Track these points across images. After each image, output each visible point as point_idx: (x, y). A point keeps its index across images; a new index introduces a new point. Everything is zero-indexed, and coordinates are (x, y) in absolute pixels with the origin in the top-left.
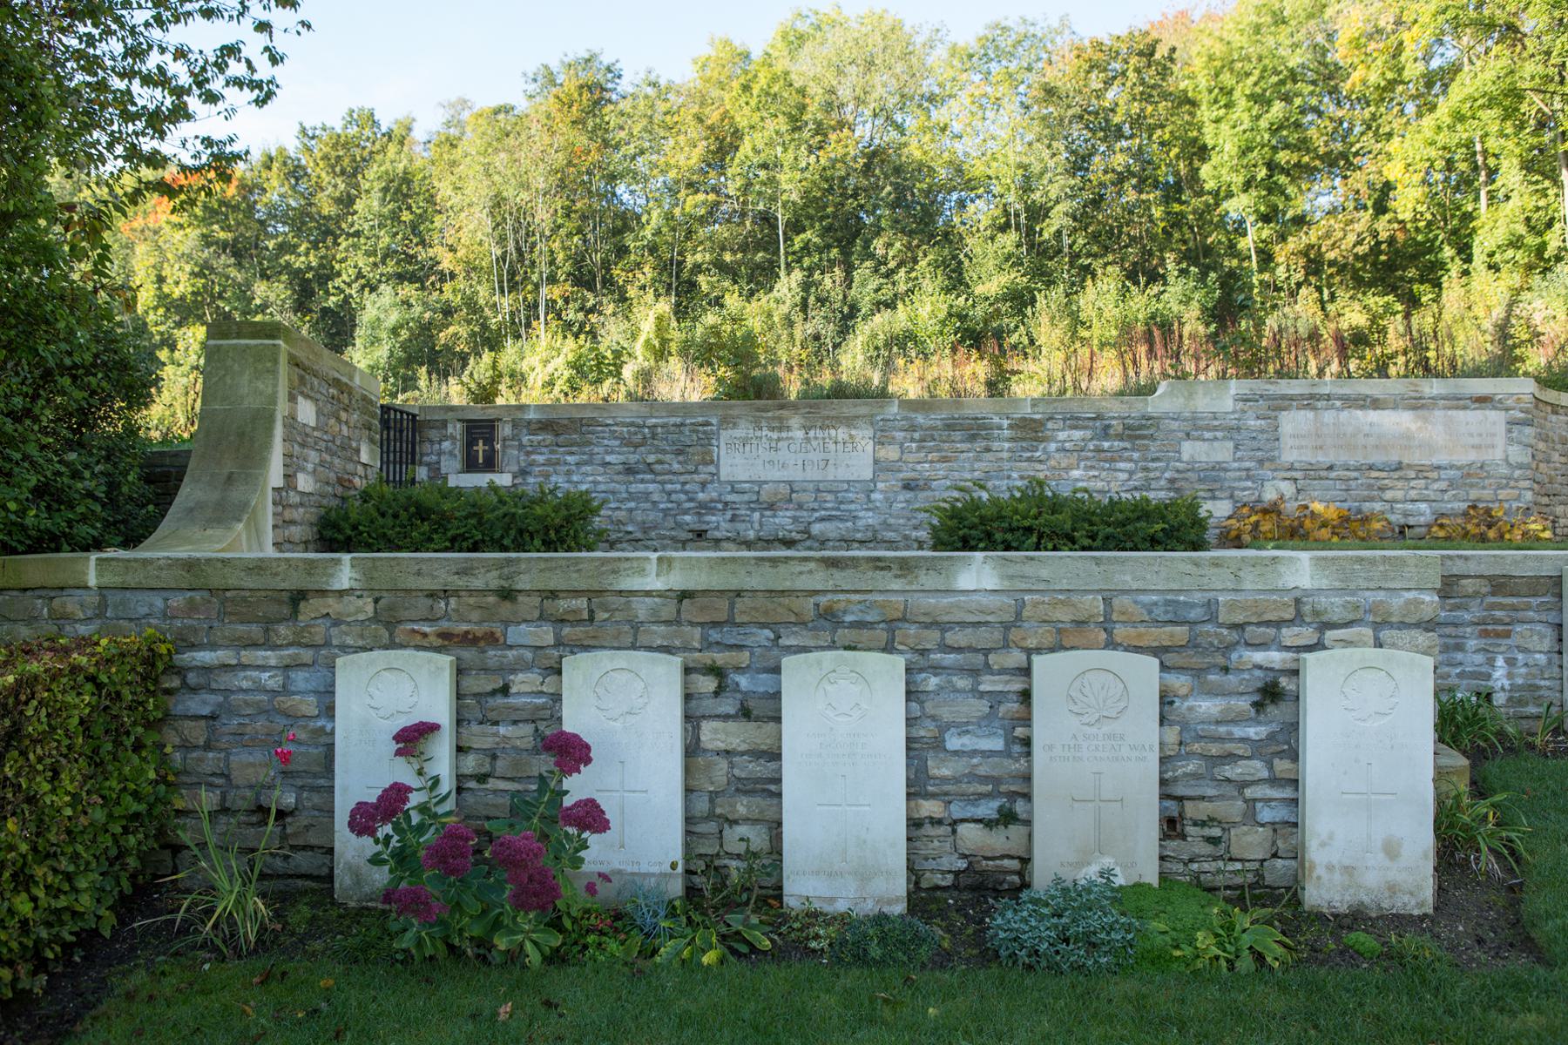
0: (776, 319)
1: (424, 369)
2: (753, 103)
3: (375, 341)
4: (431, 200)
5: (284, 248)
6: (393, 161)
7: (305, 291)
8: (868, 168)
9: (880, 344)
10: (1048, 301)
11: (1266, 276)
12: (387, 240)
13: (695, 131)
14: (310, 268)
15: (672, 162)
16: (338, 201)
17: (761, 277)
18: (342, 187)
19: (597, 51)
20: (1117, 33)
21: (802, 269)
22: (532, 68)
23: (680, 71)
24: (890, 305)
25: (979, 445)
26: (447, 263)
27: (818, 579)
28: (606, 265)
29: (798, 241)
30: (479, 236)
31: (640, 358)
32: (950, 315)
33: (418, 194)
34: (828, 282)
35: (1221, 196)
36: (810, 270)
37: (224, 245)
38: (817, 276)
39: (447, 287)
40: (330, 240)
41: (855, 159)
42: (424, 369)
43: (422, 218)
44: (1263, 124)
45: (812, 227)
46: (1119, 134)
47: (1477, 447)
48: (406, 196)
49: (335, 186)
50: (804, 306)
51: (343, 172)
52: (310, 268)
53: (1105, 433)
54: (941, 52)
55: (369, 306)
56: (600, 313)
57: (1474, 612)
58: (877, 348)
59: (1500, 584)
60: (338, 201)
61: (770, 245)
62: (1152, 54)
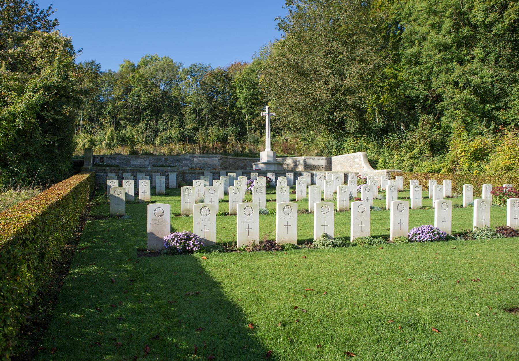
0: (139, 132)
2: (135, 81)
9: (164, 139)
10: (202, 130)
11: (250, 127)
13: (120, 86)
17: (136, 122)
19: (94, 60)
21: (146, 120)
23: (116, 69)
24: (166, 130)
28: (97, 116)
31: (107, 140)
32: (179, 133)
34: (152, 123)
35: (242, 108)
36: (148, 121)
38: (149, 122)
41: (159, 95)
44: (249, 94)
46: (219, 93)
50: (146, 129)
53: (175, 160)
54: (181, 69)
57: (197, 175)
58: (163, 140)
59: (199, 173)
61: (138, 113)
62: (227, 76)
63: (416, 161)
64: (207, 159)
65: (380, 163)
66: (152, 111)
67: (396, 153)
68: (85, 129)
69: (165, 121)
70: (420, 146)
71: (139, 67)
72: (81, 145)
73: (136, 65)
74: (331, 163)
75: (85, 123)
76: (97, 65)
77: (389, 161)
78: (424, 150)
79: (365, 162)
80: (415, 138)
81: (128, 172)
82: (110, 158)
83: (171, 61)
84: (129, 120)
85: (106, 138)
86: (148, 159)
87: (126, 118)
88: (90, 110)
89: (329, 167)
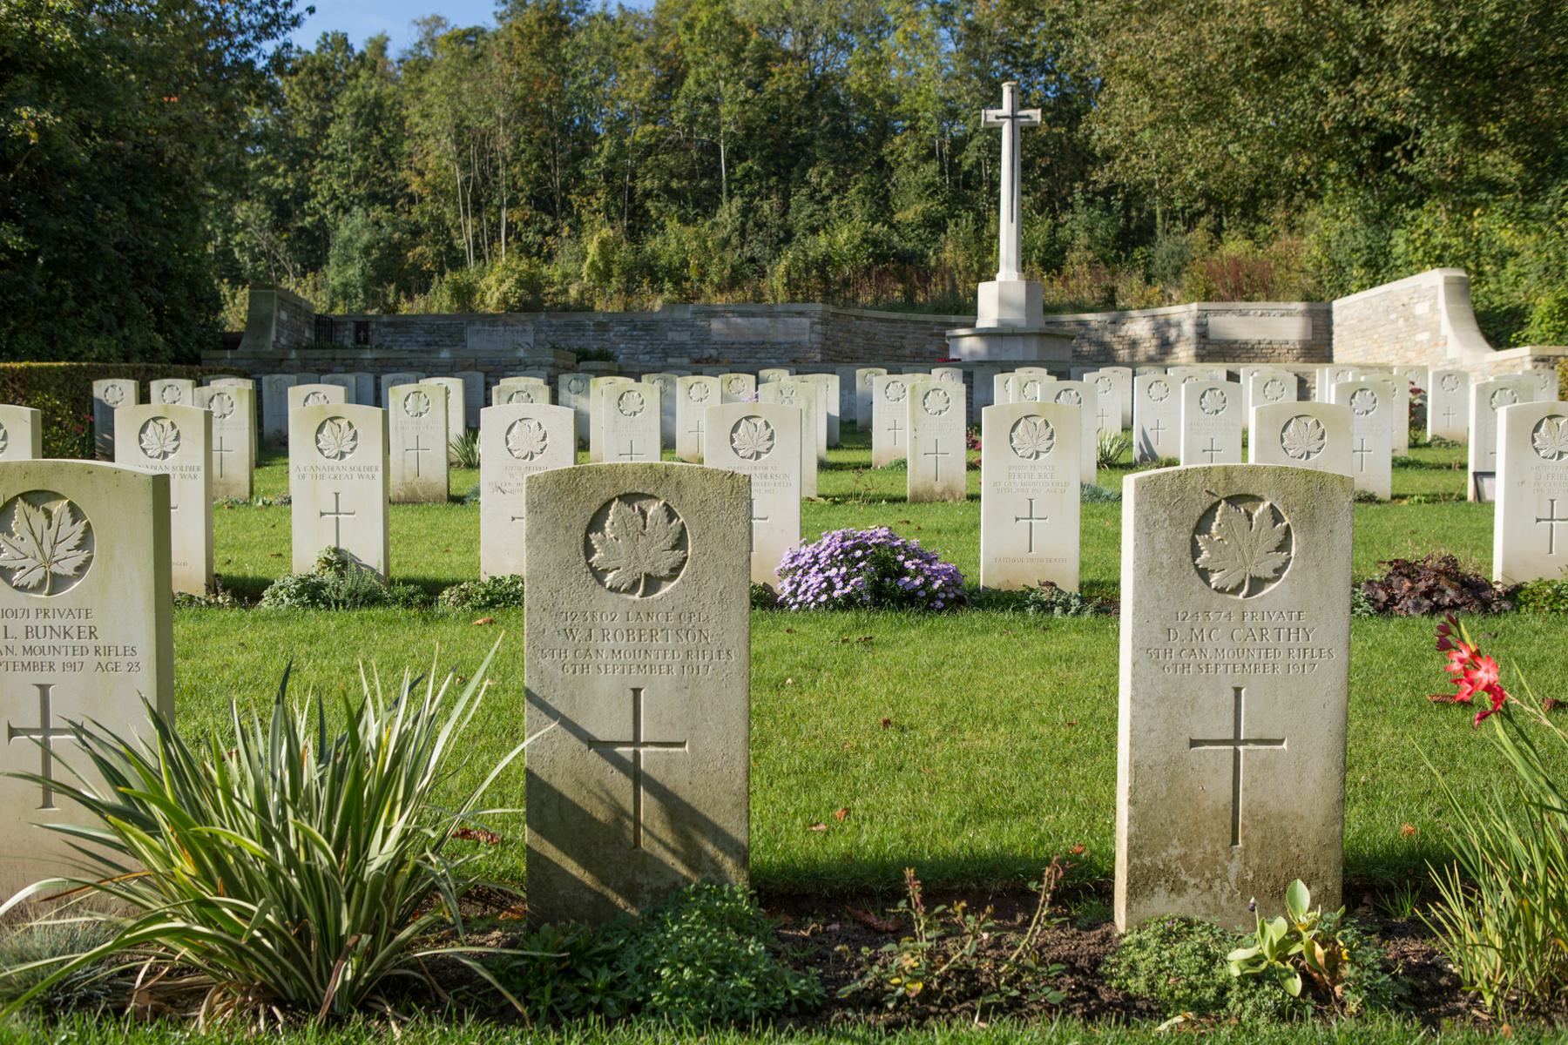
1: (393, 287)
3: (348, 260)
6: (368, 86)
7: (283, 209)
8: (810, 98)
14: (287, 189)
15: (624, 94)
16: (314, 124)
17: (706, 203)
18: (316, 111)
25: (581, 333)
26: (415, 186)
27: (408, 355)
28: (565, 188)
30: (445, 162)
31: (585, 280)
32: (865, 240)
33: (388, 119)
34: (766, 207)
38: (756, 202)
39: (415, 209)
40: (306, 164)
42: (393, 287)
43: (390, 142)
45: (753, 157)
47: (797, 334)
48: (378, 119)
49: (310, 110)
51: (317, 96)
52: (287, 189)
53: (635, 328)
55: (342, 227)
60: (314, 124)
61: (712, 171)
64: (767, 320)
65: (1536, 318)
66: (769, 158)
68: (518, 238)
69: (818, 196)
72: (495, 301)
74: (1330, 333)
75: (517, 215)
79: (1452, 319)
81: (364, 370)
84: (675, 195)
85: (585, 269)
86: (530, 328)
87: (667, 189)
88: (535, 165)
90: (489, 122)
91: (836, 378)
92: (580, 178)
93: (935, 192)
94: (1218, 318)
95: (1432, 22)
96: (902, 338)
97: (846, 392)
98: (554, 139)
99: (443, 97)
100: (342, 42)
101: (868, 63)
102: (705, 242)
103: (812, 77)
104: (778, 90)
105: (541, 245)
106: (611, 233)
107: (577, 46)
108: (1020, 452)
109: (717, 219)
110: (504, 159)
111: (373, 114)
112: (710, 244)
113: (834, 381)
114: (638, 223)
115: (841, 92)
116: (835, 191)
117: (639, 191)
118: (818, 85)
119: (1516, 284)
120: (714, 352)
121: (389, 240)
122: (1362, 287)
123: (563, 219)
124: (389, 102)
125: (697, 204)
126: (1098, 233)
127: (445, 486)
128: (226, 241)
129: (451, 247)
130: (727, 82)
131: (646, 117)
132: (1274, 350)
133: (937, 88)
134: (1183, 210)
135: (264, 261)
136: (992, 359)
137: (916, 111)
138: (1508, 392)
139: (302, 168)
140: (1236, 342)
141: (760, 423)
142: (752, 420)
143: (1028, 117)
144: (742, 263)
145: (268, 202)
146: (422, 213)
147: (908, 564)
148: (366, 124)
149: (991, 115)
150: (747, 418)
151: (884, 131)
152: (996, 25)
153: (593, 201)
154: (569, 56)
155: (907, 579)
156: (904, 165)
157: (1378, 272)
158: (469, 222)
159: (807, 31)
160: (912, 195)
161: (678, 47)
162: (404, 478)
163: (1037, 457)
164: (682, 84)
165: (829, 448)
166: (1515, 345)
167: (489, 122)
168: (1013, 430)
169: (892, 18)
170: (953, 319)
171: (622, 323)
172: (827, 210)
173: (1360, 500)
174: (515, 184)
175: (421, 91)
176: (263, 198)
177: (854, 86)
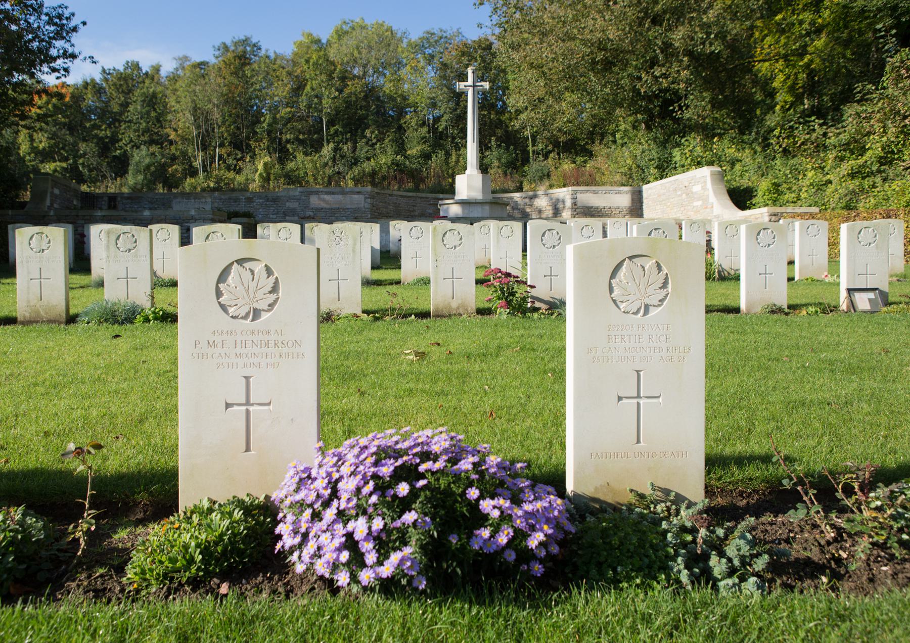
4: (165, 107)
5: (95, 126)
7: (105, 147)
8: (366, 97)
12: (144, 124)
15: (276, 93)
16: (121, 105)
17: (317, 146)
18: (123, 99)
19: (249, 36)
20: (475, 39)
21: (334, 142)
22: (218, 43)
29: (332, 130)
30: (187, 125)
32: (393, 163)
33: (159, 103)
34: (345, 148)
36: (339, 143)
37: (64, 124)
39: (173, 148)
40: (117, 124)
42: (161, 185)
45: (339, 124)
48: (155, 104)
49: (119, 98)
51: (123, 92)
52: (107, 137)
53: (268, 200)
56: (243, 161)
60: (121, 105)
63: (867, 183)
64: (340, 197)
65: (760, 193)
67: (809, 166)
68: (224, 162)
69: (370, 143)
70: (885, 139)
71: (329, 43)
73: (324, 41)
75: (223, 151)
76: (254, 45)
77: (789, 189)
78: (900, 151)
80: (868, 119)
82: (128, 198)
83: (390, 29)
84: (301, 142)
87: (297, 139)
89: (636, 209)
90: (210, 106)
91: (378, 225)
92: (255, 133)
93: (426, 141)
94: (582, 195)
95: (701, 33)
96: (414, 206)
97: (384, 235)
98: (242, 115)
99: (186, 93)
100: (136, 66)
101: (393, 81)
102: (316, 164)
103: (367, 87)
104: (351, 93)
105: (236, 166)
106: (270, 159)
107: (253, 70)
108: (622, 306)
109: (322, 153)
110: (217, 124)
111: (152, 101)
112: (318, 165)
113: (376, 227)
114: (284, 155)
115: (381, 94)
116: (378, 141)
117: (284, 140)
118: (370, 91)
119: (741, 176)
120: (311, 214)
121: (159, 163)
122: (656, 179)
123: (247, 153)
124: (160, 95)
125: (312, 146)
126: (503, 160)
127: (64, 308)
128: (75, 162)
129: (191, 166)
130: (326, 88)
131: (287, 105)
132: (612, 212)
133: (426, 92)
134: (542, 149)
135: (95, 172)
136: (465, 216)
137: (417, 103)
138: (871, 230)
139: (115, 127)
140: (592, 207)
141: (259, 268)
142: (247, 265)
143: (482, 86)
144: (334, 174)
145: (97, 144)
146: (176, 149)
147: (486, 505)
148: (148, 105)
149: (461, 86)
150: (549, 230)
151: (401, 113)
152: (454, 63)
153: (261, 144)
154: (249, 75)
155: (486, 533)
156: (411, 129)
157: (664, 171)
158: (200, 154)
159: (365, 66)
160: (415, 143)
161: (303, 72)
162: (29, 301)
163: (646, 312)
164: (304, 89)
165: (373, 268)
166: (750, 208)
167: (210, 106)
168: (613, 275)
169: (405, 61)
170: (441, 196)
171: (260, 198)
172: (375, 149)
173: (773, 312)
174: (223, 136)
175: (176, 90)
176: (95, 141)
177: (387, 91)
